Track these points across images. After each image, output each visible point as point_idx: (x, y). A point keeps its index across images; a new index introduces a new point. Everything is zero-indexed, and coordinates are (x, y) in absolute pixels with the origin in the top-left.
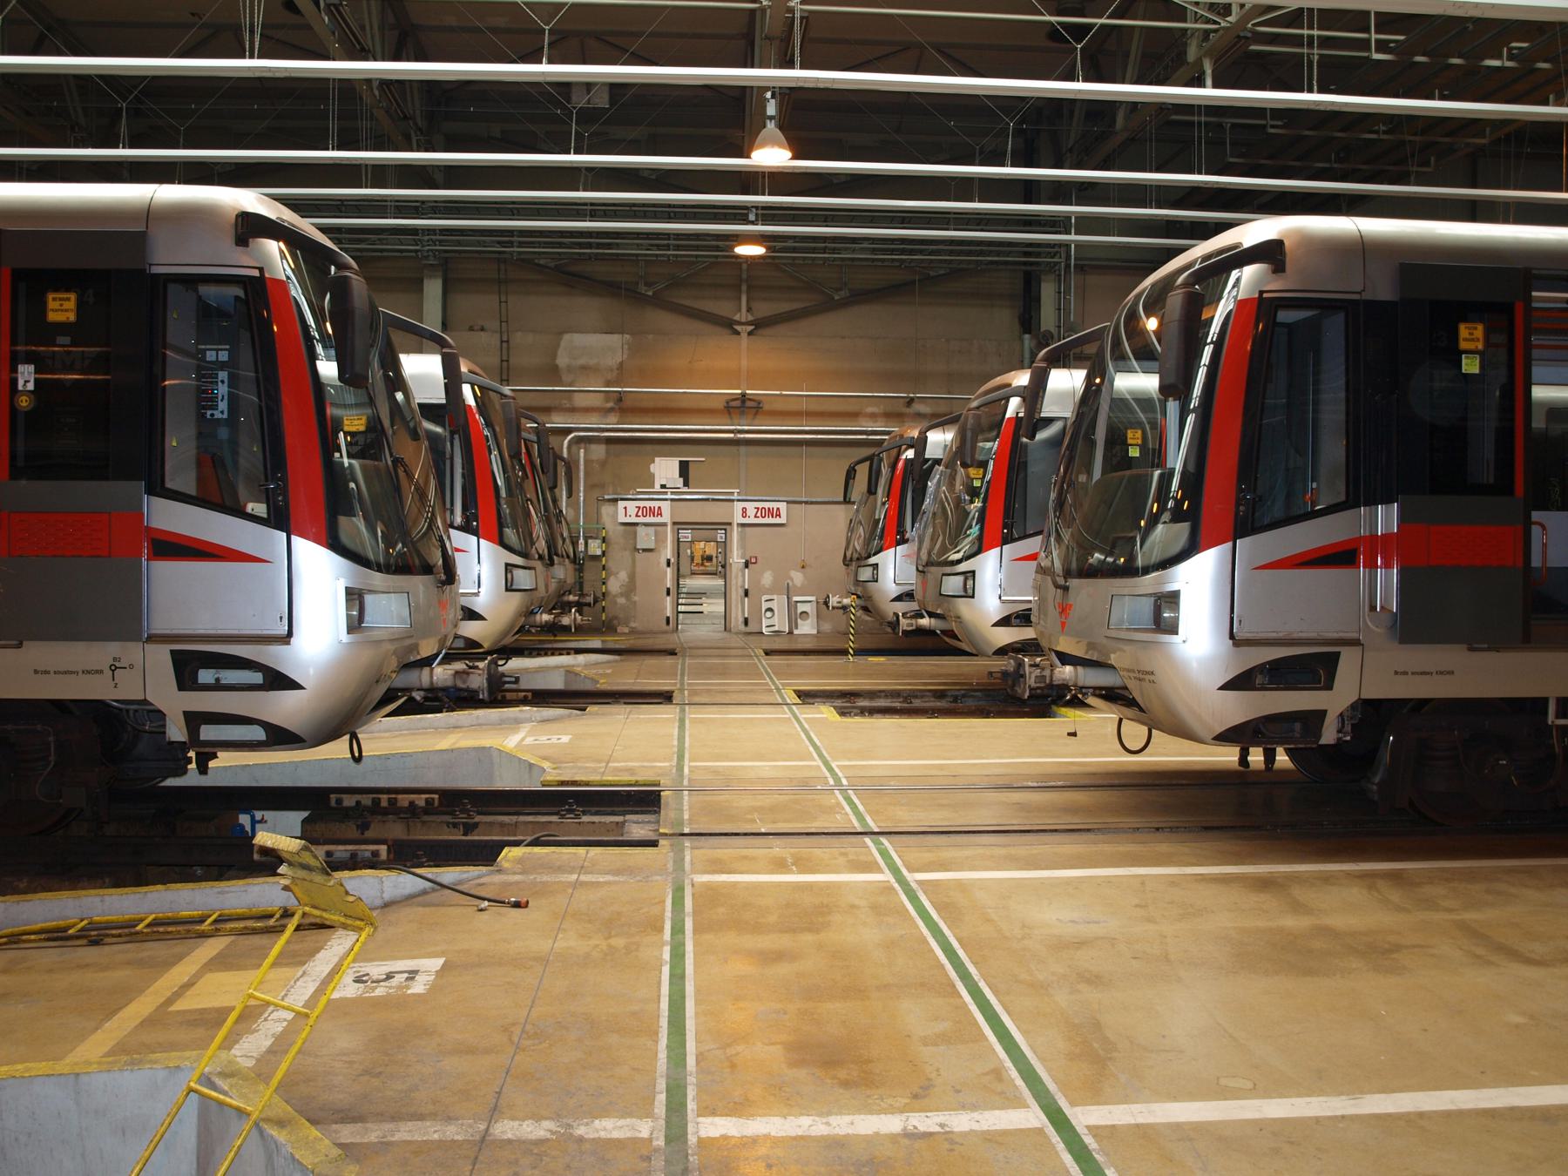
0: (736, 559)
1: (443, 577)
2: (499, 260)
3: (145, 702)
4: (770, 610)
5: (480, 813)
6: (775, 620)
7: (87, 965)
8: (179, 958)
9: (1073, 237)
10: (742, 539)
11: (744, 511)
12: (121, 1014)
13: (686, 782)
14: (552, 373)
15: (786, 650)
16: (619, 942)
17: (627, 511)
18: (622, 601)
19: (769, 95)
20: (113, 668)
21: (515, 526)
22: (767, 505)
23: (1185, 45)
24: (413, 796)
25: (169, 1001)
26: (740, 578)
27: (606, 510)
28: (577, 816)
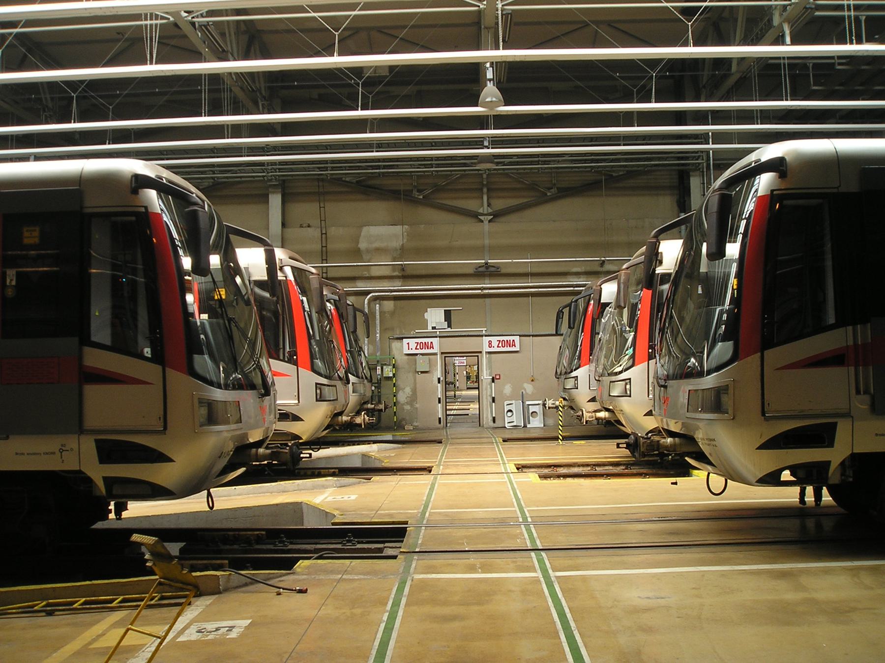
0: (485, 376)
1: (263, 391)
2: (318, 180)
3: (80, 472)
4: (510, 411)
5: (291, 543)
6: (514, 418)
7: (45, 626)
8: (98, 622)
9: (711, 146)
10: (489, 362)
11: (490, 343)
12: (62, 650)
13: (425, 522)
14: (356, 253)
15: (521, 437)
16: (358, 611)
17: (410, 346)
18: (408, 407)
19: (488, 65)
20: (61, 451)
21: (323, 359)
22: (505, 338)
23: (772, 15)
25: (90, 643)
26: (488, 389)
27: (395, 345)
28: (354, 545)
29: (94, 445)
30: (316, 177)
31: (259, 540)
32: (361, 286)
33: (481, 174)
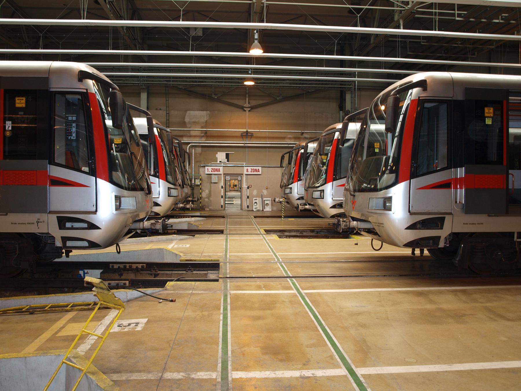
0: (245, 186)
1: (147, 192)
2: (166, 86)
3: (48, 233)
4: (256, 203)
5: (159, 270)
6: (258, 206)
7: (29, 321)
8: (59, 319)
9: (356, 79)
10: (247, 179)
11: (247, 170)
12: (40, 337)
13: (228, 260)
14: (183, 124)
15: (261, 216)
16: (206, 313)
17: (208, 170)
18: (207, 200)
19: (255, 32)
20: (38, 222)
21: (171, 175)
22: (255, 168)
23: (394, 15)
24: (137, 265)
25: (56, 333)
26: (246, 192)
27: (201, 169)
28: (192, 271)
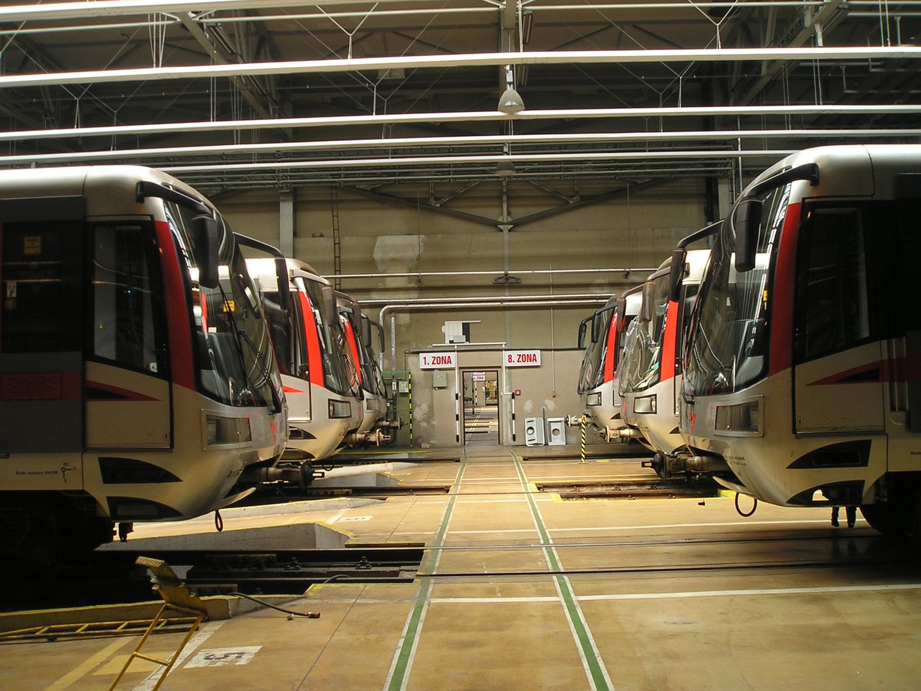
0: (505, 392)
1: (274, 408)
2: (331, 187)
3: (83, 492)
4: (531, 428)
5: (303, 566)
6: (535, 436)
7: (47, 652)
8: (102, 648)
9: (740, 152)
10: (509, 377)
11: (510, 357)
12: (64, 677)
13: (442, 544)
14: (370, 264)
15: (542, 456)
16: (372, 637)
17: (426, 360)
18: (424, 424)
19: (508, 68)
20: (64, 470)
21: (336, 375)
22: (526, 353)
23: (803, 15)
25: (94, 670)
26: (508, 406)
27: (411, 359)
28: (368, 568)
29: (97, 463)
30: (329, 184)
31: (269, 563)
32: (376, 298)
33: (501, 182)
